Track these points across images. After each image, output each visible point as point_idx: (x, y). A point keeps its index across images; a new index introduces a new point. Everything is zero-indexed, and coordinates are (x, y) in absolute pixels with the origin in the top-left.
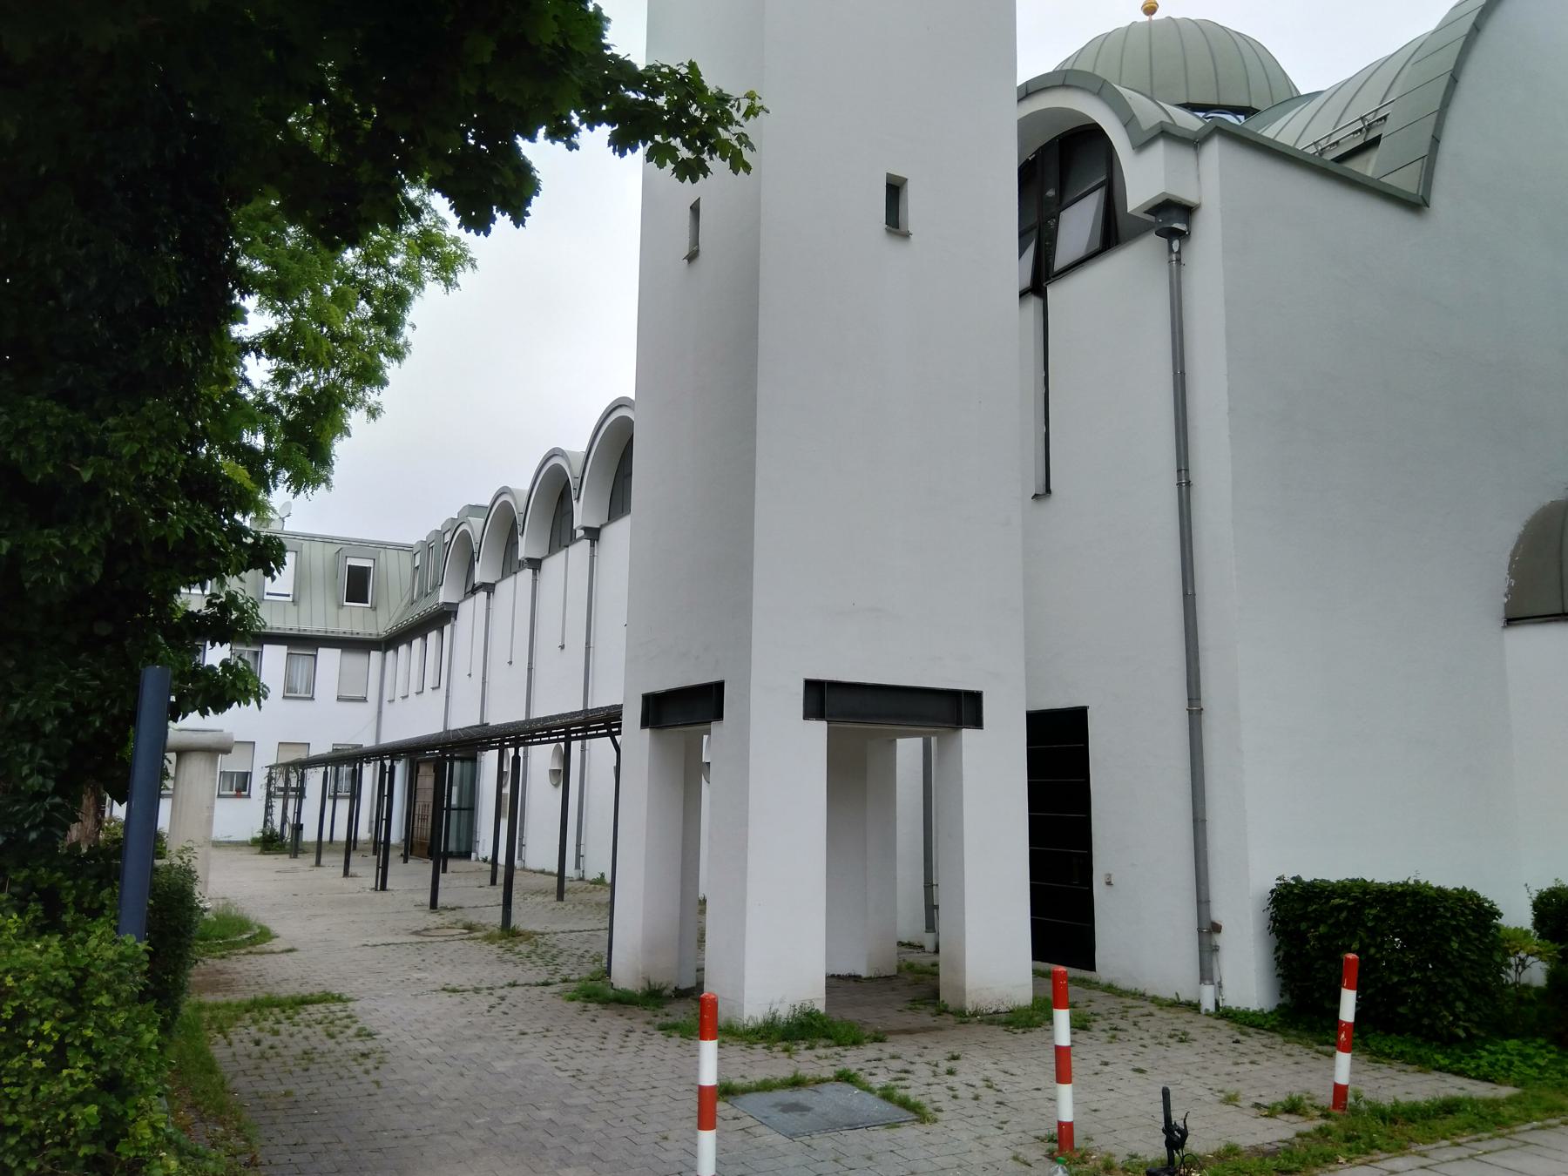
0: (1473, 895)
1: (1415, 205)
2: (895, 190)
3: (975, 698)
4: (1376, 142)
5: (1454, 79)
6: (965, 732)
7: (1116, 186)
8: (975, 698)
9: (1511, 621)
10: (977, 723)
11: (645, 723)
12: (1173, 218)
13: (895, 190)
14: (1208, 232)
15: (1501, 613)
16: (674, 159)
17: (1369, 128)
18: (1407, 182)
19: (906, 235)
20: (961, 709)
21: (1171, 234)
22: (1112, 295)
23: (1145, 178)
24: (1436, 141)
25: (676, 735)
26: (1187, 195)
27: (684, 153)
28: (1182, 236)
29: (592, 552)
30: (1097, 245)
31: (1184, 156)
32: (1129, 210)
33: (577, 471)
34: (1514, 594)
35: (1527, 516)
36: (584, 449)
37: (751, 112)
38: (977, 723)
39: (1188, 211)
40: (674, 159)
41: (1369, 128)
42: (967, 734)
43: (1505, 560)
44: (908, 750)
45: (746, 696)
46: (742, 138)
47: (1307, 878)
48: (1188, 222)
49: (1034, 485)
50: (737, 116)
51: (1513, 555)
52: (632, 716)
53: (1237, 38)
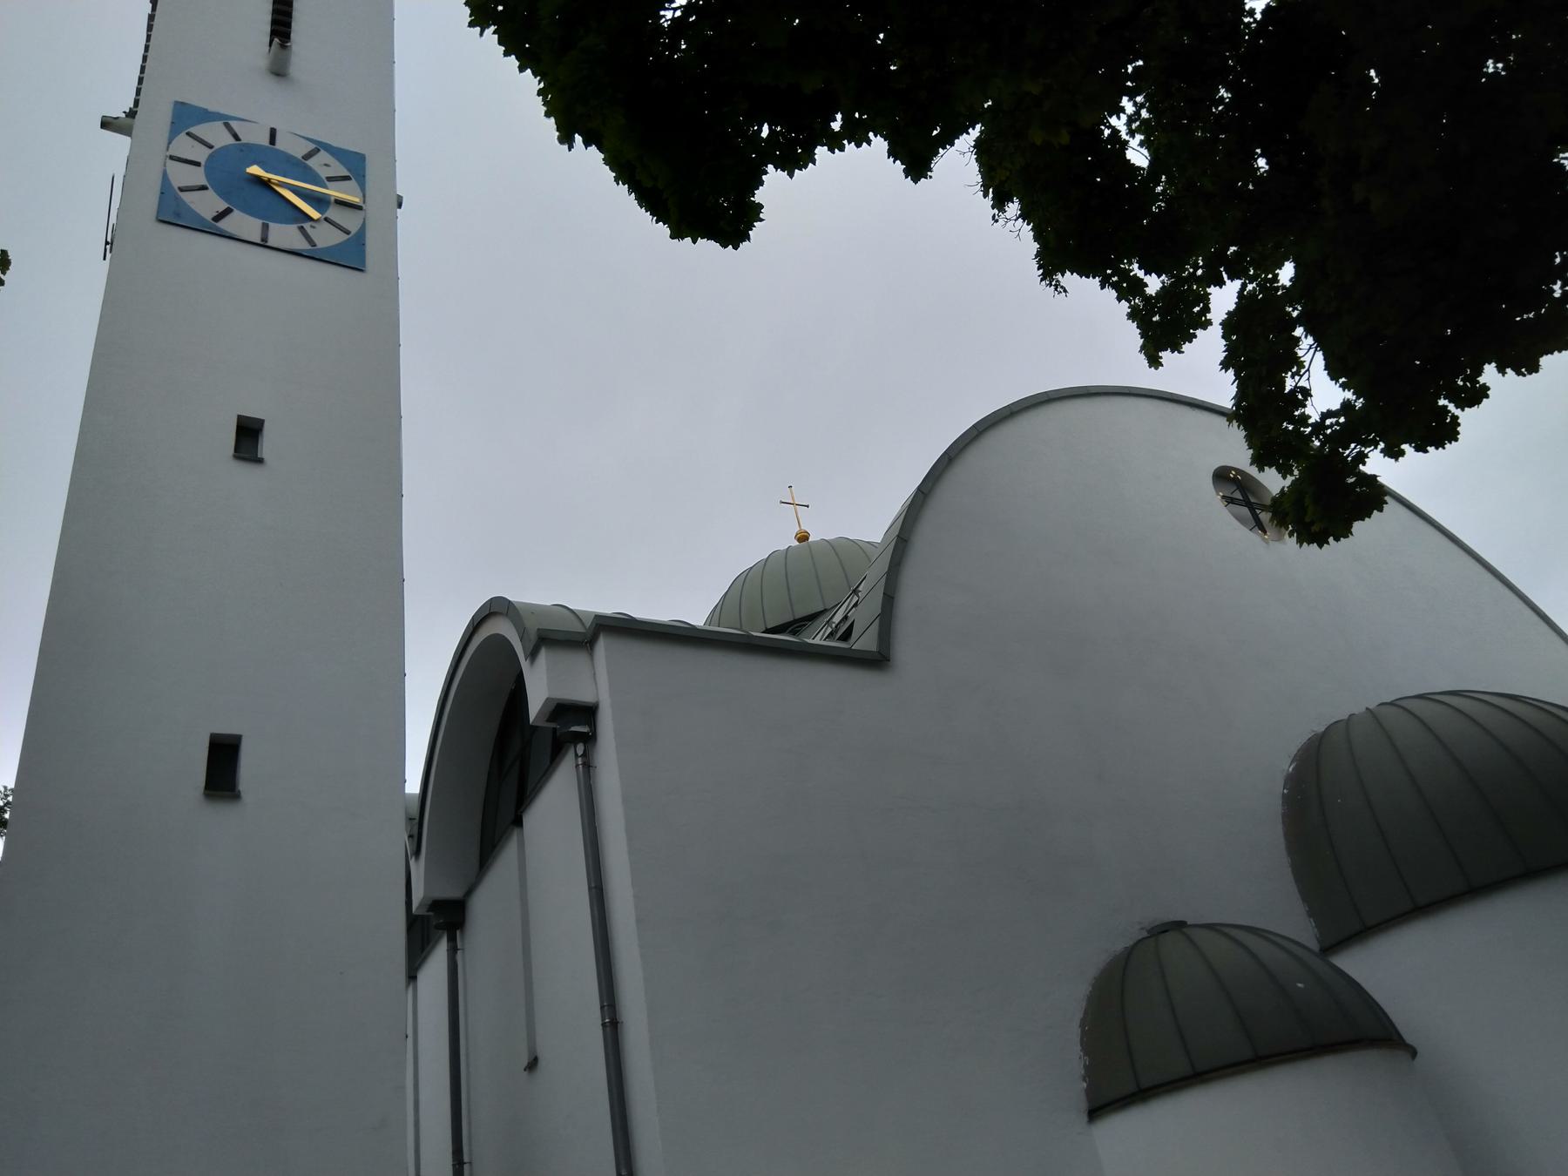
1: (878, 661)
9: (1096, 1112)
15: (1084, 1105)
26: (582, 695)
34: (1094, 1073)
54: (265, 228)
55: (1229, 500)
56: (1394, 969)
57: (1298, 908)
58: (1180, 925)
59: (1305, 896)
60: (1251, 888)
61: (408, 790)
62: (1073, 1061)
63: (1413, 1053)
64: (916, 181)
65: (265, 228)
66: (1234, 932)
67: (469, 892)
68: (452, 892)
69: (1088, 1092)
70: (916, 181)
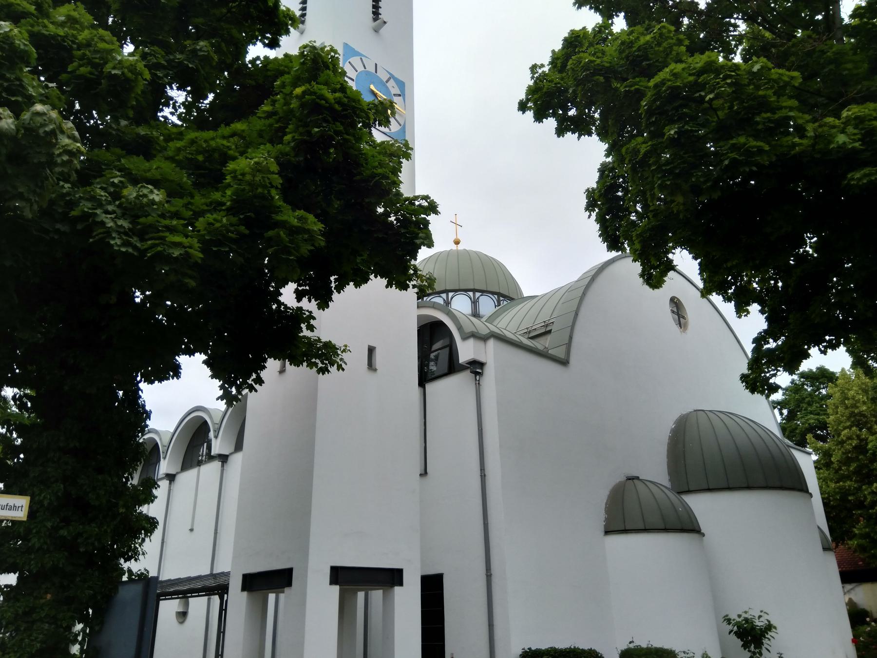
0: (595, 651)
1: (564, 362)
2: (371, 350)
3: (400, 572)
4: (550, 332)
5: (577, 314)
6: (396, 588)
7: (454, 347)
8: (400, 572)
9: (607, 532)
10: (401, 584)
11: (244, 589)
12: (476, 367)
13: (371, 350)
14: (490, 373)
15: (602, 529)
16: (317, 367)
17: (547, 326)
18: (560, 353)
19: (375, 370)
20: (394, 577)
21: (476, 373)
22: (449, 390)
23: (466, 351)
24: (571, 338)
25: (258, 595)
26: (482, 359)
27: (320, 365)
28: (480, 374)
29: (170, 487)
30: (446, 371)
31: (480, 344)
32: (461, 361)
33: (166, 442)
34: (608, 521)
35: (610, 487)
36: (172, 430)
37: (344, 351)
38: (401, 584)
39: (481, 365)
40: (317, 367)
41: (547, 326)
42: (397, 589)
43: (603, 506)
44: (377, 595)
45: (305, 576)
46: (341, 360)
47: (533, 649)
48: (482, 369)
49: (419, 469)
50: (339, 352)
51: (606, 504)
52: (235, 584)
53: (496, 265)
54: (387, 81)
55: (673, 312)
56: (702, 506)
57: (667, 477)
58: (638, 478)
59: (670, 474)
60: (655, 469)
61: (21, 515)
62: (602, 515)
63: (703, 535)
64: (559, 136)
65: (387, 81)
66: (648, 483)
67: (178, 473)
68: (173, 472)
69: (605, 526)
70: (559, 136)
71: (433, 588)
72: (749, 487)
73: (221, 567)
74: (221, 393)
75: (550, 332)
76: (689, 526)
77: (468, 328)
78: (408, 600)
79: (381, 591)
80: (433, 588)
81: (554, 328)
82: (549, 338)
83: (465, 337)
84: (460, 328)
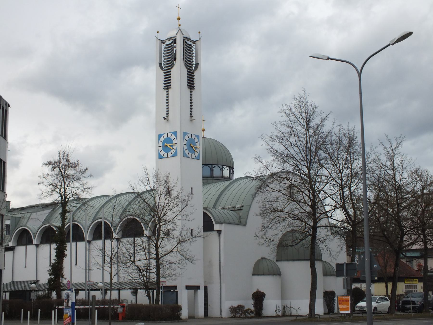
4: (242, 210)
9: (253, 275)
12: (219, 232)
31: (221, 225)
42: (199, 290)
53: (222, 146)
66: (267, 261)
71: (206, 288)
72: (299, 260)
73: (74, 244)
74: (72, 161)
75: (242, 210)
76: (277, 273)
77: (218, 220)
78: (201, 292)
79: (194, 290)
80: (206, 288)
81: (243, 208)
82: (241, 211)
83: (217, 223)
84: (215, 220)
